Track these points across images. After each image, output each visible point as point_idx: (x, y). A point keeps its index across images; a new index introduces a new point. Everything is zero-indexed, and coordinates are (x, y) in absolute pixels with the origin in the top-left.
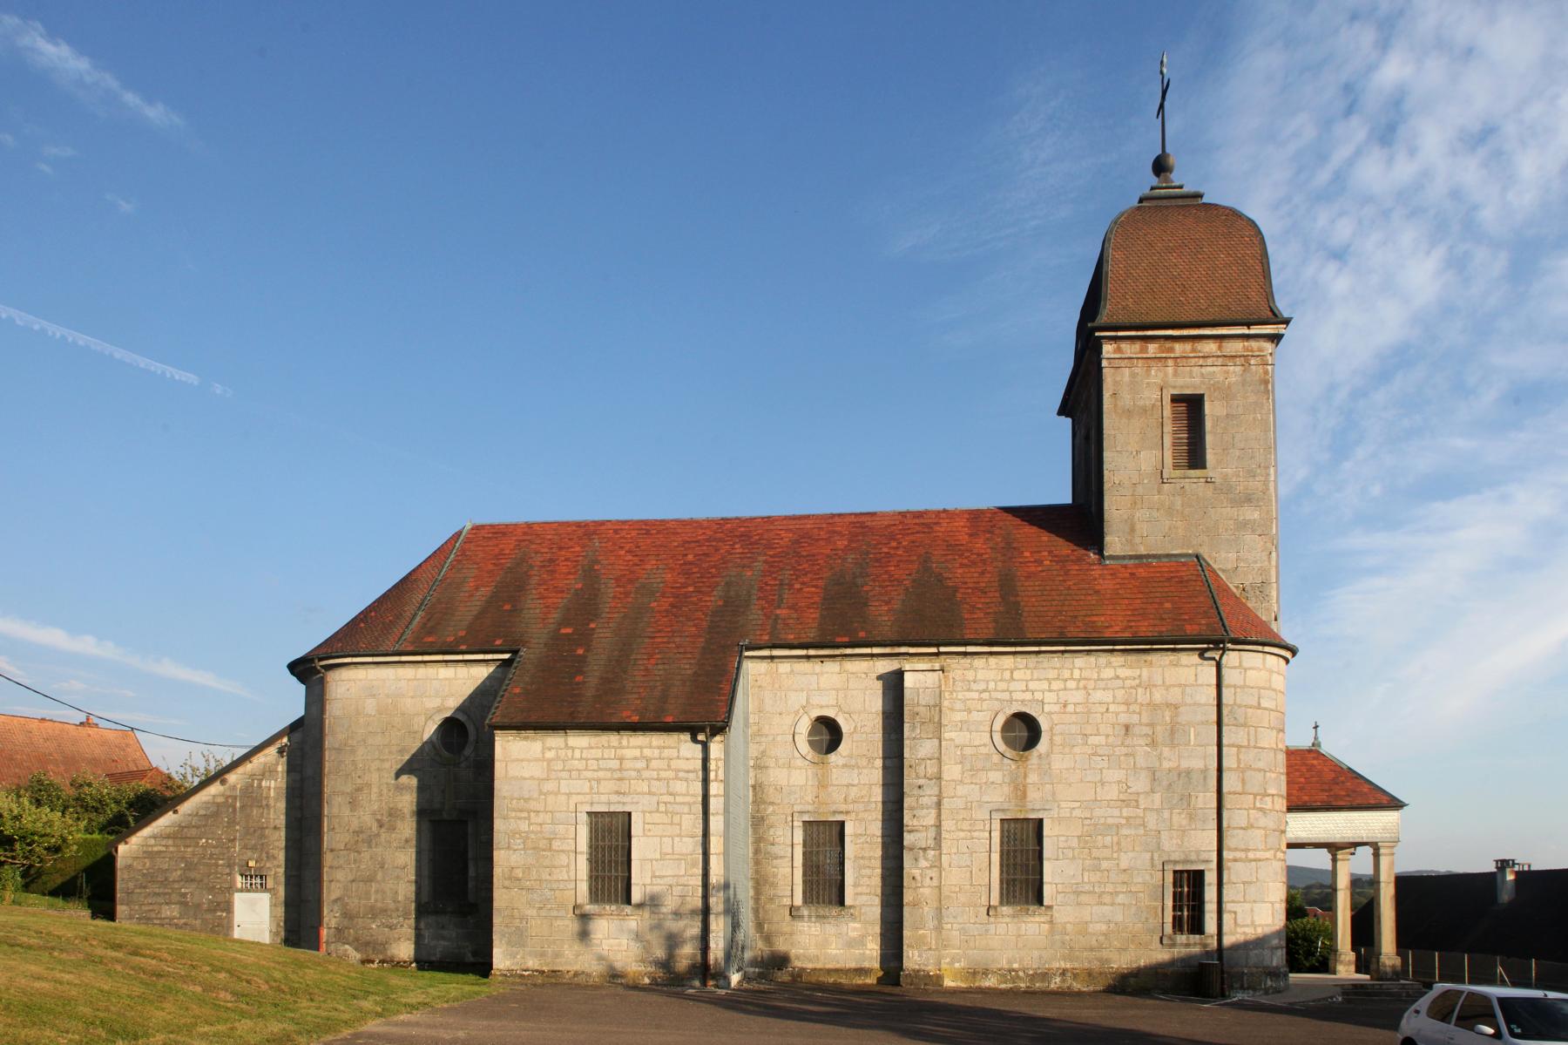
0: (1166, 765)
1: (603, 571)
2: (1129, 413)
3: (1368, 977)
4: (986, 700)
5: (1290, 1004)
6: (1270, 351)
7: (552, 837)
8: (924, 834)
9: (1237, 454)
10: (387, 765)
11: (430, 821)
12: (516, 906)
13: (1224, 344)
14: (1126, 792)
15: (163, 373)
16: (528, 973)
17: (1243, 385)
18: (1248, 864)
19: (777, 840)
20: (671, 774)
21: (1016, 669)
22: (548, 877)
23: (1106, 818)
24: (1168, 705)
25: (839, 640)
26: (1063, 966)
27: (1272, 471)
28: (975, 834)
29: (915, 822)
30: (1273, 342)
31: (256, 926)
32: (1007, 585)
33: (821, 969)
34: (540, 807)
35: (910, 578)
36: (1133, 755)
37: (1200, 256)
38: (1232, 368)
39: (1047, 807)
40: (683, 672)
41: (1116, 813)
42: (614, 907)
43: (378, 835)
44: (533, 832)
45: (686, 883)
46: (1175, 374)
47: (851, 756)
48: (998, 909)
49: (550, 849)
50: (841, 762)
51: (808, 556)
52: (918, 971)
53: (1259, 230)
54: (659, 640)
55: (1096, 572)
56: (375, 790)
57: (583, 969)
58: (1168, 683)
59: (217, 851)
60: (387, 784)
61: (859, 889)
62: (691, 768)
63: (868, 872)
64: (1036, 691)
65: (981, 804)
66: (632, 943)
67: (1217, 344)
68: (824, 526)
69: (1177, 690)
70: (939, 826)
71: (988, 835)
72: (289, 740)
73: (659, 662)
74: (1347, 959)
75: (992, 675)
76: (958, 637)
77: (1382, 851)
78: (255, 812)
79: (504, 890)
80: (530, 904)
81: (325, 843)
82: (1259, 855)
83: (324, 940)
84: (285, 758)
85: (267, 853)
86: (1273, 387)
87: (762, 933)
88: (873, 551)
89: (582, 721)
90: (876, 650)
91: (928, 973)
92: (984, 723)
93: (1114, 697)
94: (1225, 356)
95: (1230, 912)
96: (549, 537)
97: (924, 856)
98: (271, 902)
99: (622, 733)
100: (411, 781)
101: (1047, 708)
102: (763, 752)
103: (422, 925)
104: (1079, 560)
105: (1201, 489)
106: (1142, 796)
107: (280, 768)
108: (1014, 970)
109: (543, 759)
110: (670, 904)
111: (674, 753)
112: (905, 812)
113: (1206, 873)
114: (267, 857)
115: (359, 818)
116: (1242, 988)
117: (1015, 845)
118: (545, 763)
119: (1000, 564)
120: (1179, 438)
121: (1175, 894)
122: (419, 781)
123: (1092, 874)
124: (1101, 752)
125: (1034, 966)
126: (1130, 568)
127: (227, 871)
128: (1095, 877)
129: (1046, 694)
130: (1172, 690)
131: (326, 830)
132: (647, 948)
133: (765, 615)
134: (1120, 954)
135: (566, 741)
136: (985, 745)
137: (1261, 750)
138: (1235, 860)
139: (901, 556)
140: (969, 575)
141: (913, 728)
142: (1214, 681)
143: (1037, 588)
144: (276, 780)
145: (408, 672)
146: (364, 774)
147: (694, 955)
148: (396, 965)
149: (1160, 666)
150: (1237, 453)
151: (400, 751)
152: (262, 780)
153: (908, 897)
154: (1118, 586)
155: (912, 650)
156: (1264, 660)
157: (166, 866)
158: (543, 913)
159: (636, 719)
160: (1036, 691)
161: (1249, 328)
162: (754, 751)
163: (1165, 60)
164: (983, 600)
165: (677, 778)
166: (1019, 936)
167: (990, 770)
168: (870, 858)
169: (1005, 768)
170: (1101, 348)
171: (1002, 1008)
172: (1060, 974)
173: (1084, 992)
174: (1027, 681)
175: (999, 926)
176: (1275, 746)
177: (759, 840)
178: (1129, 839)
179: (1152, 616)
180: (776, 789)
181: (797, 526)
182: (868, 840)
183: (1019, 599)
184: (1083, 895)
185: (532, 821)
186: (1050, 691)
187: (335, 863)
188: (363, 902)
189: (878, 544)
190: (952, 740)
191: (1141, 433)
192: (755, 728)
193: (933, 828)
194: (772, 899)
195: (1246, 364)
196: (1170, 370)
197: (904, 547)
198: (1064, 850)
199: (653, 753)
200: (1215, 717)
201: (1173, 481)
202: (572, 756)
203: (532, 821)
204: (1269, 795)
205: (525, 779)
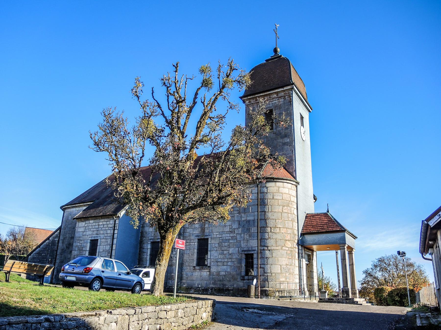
0: (243, 219)
14: (231, 229)
23: (226, 237)
26: (212, 286)
36: (234, 217)
38: (281, 100)
39: (210, 234)
41: (229, 235)
43: (66, 250)
49: (82, 250)
56: (67, 239)
65: (193, 234)
106: (236, 230)
108: (199, 288)
111: (108, 223)
137: (274, 213)
172: (211, 289)
184: (219, 262)
205: (80, 232)
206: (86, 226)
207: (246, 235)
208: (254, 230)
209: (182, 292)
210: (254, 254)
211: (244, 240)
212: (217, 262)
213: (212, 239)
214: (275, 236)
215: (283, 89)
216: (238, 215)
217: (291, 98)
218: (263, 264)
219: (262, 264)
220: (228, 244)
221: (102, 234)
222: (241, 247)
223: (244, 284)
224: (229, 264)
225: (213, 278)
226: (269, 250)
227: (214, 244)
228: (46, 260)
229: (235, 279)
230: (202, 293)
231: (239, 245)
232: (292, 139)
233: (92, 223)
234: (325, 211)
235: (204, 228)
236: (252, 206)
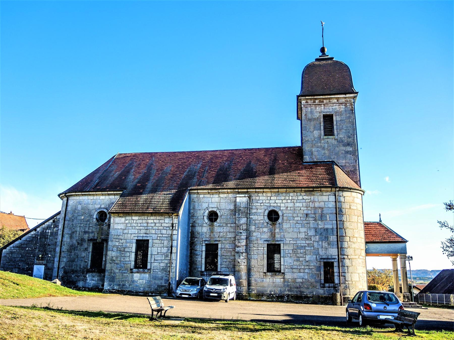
0: (320, 227)
8: (242, 248)
20: (162, 228)
21: (272, 196)
23: (301, 244)
24: (320, 208)
26: (288, 293)
28: (259, 248)
29: (239, 244)
36: (309, 223)
38: (341, 107)
39: (282, 240)
41: (304, 242)
43: (77, 247)
46: (324, 108)
49: (124, 251)
51: (214, 162)
56: (78, 233)
58: (319, 201)
61: (222, 266)
65: (261, 239)
69: (323, 203)
75: (264, 198)
80: (117, 269)
85: (45, 253)
93: (303, 205)
101: (281, 208)
108: (271, 294)
111: (162, 221)
114: (45, 254)
118: (125, 224)
128: (298, 263)
130: (321, 203)
135: (132, 217)
137: (351, 222)
144: (51, 230)
145: (91, 197)
146: (75, 228)
149: (317, 196)
157: (15, 256)
158: (121, 271)
167: (263, 228)
175: (267, 279)
177: (191, 250)
178: (308, 251)
182: (226, 250)
186: (282, 203)
192: (192, 214)
193: (245, 246)
196: (323, 107)
205: (119, 229)
206: (127, 223)
208: (333, 238)
209: (252, 299)
210: (334, 262)
211: (322, 248)
213: (285, 245)
214: (353, 246)
215: (345, 96)
216: (314, 222)
217: (353, 106)
218: (344, 272)
219: (343, 273)
220: (304, 250)
222: (318, 254)
223: (325, 292)
224: (306, 271)
225: (288, 286)
226: (349, 259)
227: (287, 250)
228: (34, 256)
229: (314, 287)
230: (276, 300)
231: (317, 253)
232: (355, 148)
233: (136, 220)
234: (378, 220)
235: (275, 233)
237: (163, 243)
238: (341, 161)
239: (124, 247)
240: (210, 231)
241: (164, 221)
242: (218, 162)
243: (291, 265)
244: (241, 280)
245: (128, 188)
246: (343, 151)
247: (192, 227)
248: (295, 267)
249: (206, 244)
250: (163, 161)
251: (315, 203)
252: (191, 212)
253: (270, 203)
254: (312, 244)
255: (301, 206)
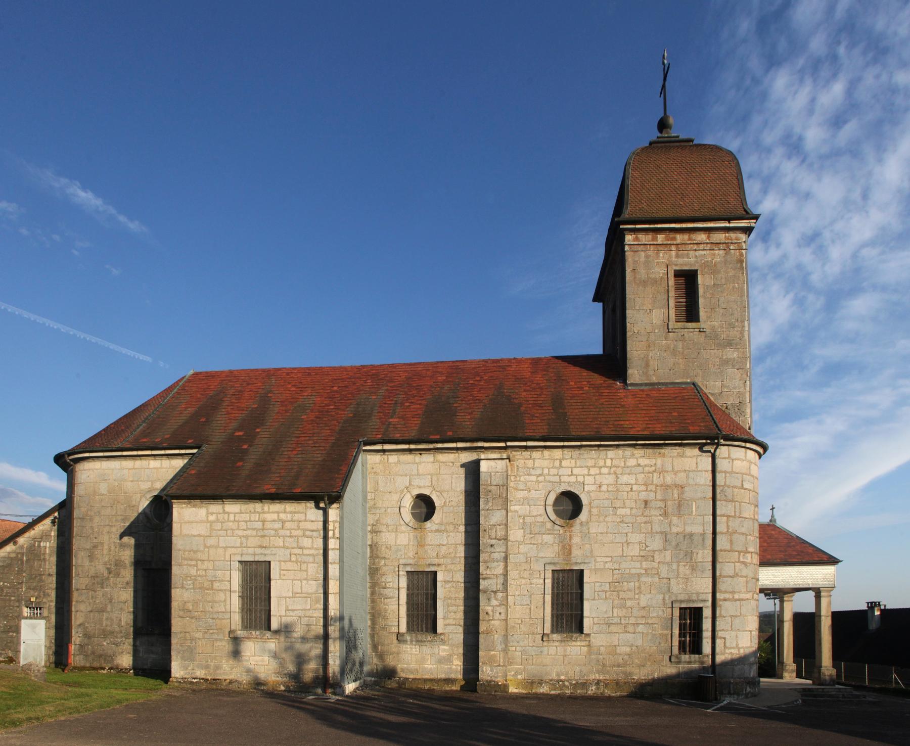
0: (675, 530)
1: (273, 397)
2: (644, 283)
3: (810, 682)
4: (542, 482)
5: (768, 707)
6: (744, 240)
7: (213, 579)
9: (721, 312)
10: (114, 529)
11: (143, 569)
12: (187, 630)
13: (711, 235)
15: (134, 356)
16: (196, 680)
17: (725, 264)
18: (734, 603)
19: (387, 585)
20: (300, 533)
21: (564, 459)
22: (210, 609)
23: (630, 569)
24: (676, 486)
25: (432, 437)
26: (598, 678)
27: (746, 323)
28: (534, 581)
30: (746, 233)
31: (35, 642)
32: (558, 402)
33: (419, 679)
34: (205, 557)
35: (487, 398)
36: (650, 522)
37: (693, 174)
38: (717, 252)
39: (586, 561)
40: (316, 459)
41: (638, 565)
42: (258, 633)
43: (108, 579)
44: (199, 576)
45: (311, 615)
46: (677, 256)
47: (441, 523)
48: (550, 636)
49: (212, 589)
50: (434, 527)
52: (490, 681)
53: (735, 156)
54: (303, 439)
55: (622, 393)
56: (106, 547)
57: (236, 678)
58: (676, 469)
59: (10, 591)
60: (114, 543)
61: (448, 621)
62: (315, 528)
63: (454, 608)
64: (579, 475)
65: (537, 559)
66: (272, 660)
67: (707, 235)
68: (430, 368)
69: (683, 475)
70: (505, 575)
71: (542, 581)
72: (59, 514)
73: (300, 452)
74: (791, 668)
75: (545, 463)
76: (521, 435)
77: (822, 594)
78: (36, 563)
79: (179, 619)
81: (73, 585)
82: (743, 596)
83: (72, 653)
84: (56, 526)
85: (44, 592)
86: (746, 265)
87: (377, 652)
88: (462, 383)
89: (234, 492)
90: (460, 445)
91: (498, 683)
92: (540, 499)
93: (636, 479)
94: (712, 243)
95: (721, 638)
96: (242, 378)
97: (495, 597)
98: (46, 625)
99: (264, 501)
100: (130, 541)
101: (587, 488)
102: (377, 520)
103: (138, 643)
104: (609, 387)
105: (696, 336)
106: (657, 553)
107: (52, 534)
108: (561, 681)
109: (207, 521)
110: (298, 632)
111: (302, 517)
112: (481, 564)
113: (704, 609)
114: (44, 595)
115: (95, 567)
116: (729, 693)
117: (563, 589)
118: (208, 524)
119: (553, 390)
120: (680, 302)
121: (680, 625)
122: (135, 541)
123: (619, 610)
124: (627, 521)
125: (576, 678)
126: (646, 391)
127: (17, 604)
128: (622, 613)
129: (586, 477)
131: (74, 576)
132: (282, 665)
133: (381, 422)
134: (640, 669)
135: (223, 508)
136: (540, 515)
137: (743, 519)
138: (725, 600)
139: (482, 385)
140: (530, 396)
141: (487, 502)
142: (710, 468)
143: (579, 404)
144: (50, 542)
145: (128, 463)
147: (317, 670)
148: (119, 672)
150: (721, 311)
151: (123, 520)
152: (41, 542)
153: (483, 627)
154: (638, 402)
155: (487, 445)
156: (746, 453)
158: (207, 636)
159: (273, 490)
160: (579, 475)
161: (729, 223)
162: (371, 519)
163: (666, 54)
164: (540, 412)
165: (304, 536)
166: (565, 656)
167: (544, 534)
168: (455, 599)
169: (556, 532)
170: (625, 238)
171: (551, 716)
172: (596, 683)
173: (613, 697)
174: (572, 468)
176: (752, 517)
177: (374, 585)
179: (663, 421)
180: (387, 547)
181: (412, 369)
182: (454, 585)
183: (566, 411)
185: (199, 567)
186: (589, 475)
187: (80, 599)
188: (98, 626)
189: (467, 378)
190: (516, 511)
191: (653, 297)
192: (372, 503)
194: (384, 628)
195: (727, 249)
196: (673, 253)
197: (486, 380)
198: (599, 593)
199: (287, 517)
200: (710, 495)
201: (676, 330)
202: (228, 519)
203: (199, 567)
204: (749, 552)
205: (194, 536)
206: (214, 522)
207: (684, 566)
212: (609, 624)
216: (662, 518)
221: (279, 547)
227: (597, 584)
232: (743, 353)
235: (570, 546)
236: (697, 501)
237: (305, 571)
238: (712, 383)
239: (210, 578)
240: (416, 543)
241: (306, 516)
242: (424, 385)
243: (606, 616)
244: (492, 653)
245: (214, 440)
246: (718, 360)
247: (372, 533)
248: (616, 621)
249: (407, 572)
250: (294, 386)
251: (665, 474)
252: (369, 498)
253: (560, 476)
254: (655, 568)
255: (634, 482)
